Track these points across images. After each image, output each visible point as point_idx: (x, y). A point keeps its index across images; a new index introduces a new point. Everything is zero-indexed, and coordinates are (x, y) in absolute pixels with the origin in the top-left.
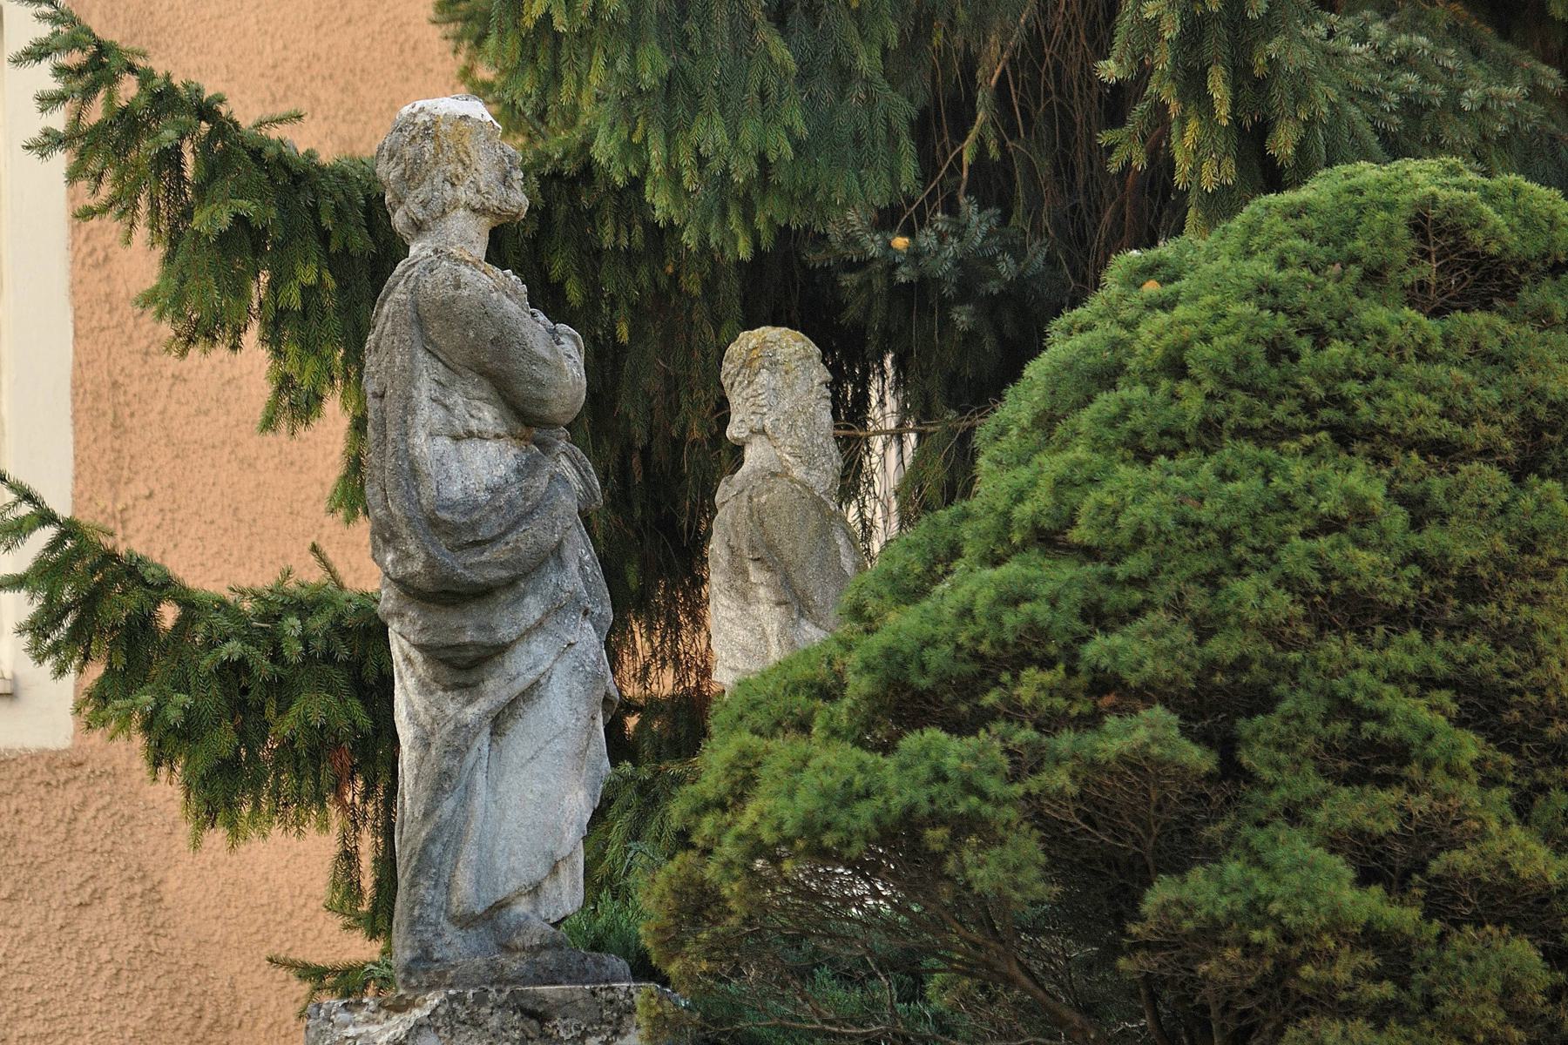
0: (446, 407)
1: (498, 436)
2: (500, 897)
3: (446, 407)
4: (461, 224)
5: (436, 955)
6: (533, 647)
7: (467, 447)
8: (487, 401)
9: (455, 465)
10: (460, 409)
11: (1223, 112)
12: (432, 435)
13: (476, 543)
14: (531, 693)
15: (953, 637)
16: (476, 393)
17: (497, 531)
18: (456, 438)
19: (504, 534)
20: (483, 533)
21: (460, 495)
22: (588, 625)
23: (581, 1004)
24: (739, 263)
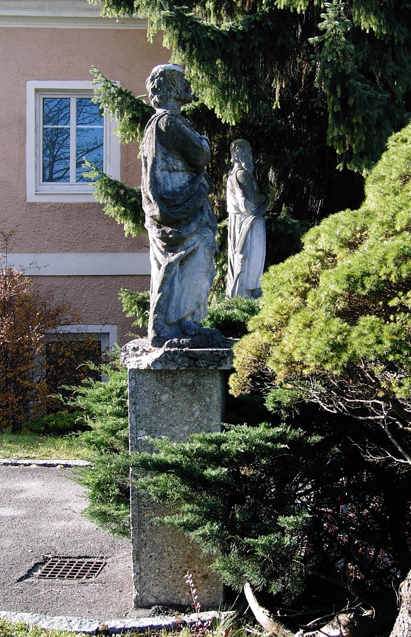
0: (166, 161)
1: (183, 171)
2: (182, 317)
3: (166, 161)
4: (172, 104)
5: (162, 336)
6: (193, 238)
7: (173, 174)
8: (180, 159)
9: (169, 180)
10: (171, 162)
11: (339, 94)
12: (162, 170)
13: (176, 205)
14: (193, 253)
15: (377, 273)
16: (176, 157)
17: (182, 202)
18: (170, 171)
19: (184, 203)
20: (178, 202)
21: (171, 189)
22: (211, 231)
23: (207, 355)
24: (233, 126)
